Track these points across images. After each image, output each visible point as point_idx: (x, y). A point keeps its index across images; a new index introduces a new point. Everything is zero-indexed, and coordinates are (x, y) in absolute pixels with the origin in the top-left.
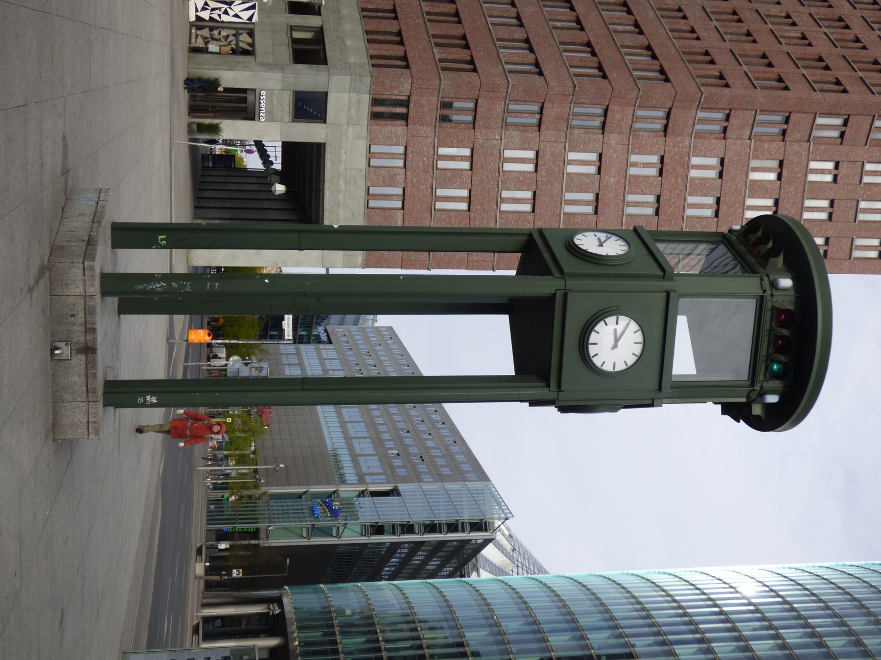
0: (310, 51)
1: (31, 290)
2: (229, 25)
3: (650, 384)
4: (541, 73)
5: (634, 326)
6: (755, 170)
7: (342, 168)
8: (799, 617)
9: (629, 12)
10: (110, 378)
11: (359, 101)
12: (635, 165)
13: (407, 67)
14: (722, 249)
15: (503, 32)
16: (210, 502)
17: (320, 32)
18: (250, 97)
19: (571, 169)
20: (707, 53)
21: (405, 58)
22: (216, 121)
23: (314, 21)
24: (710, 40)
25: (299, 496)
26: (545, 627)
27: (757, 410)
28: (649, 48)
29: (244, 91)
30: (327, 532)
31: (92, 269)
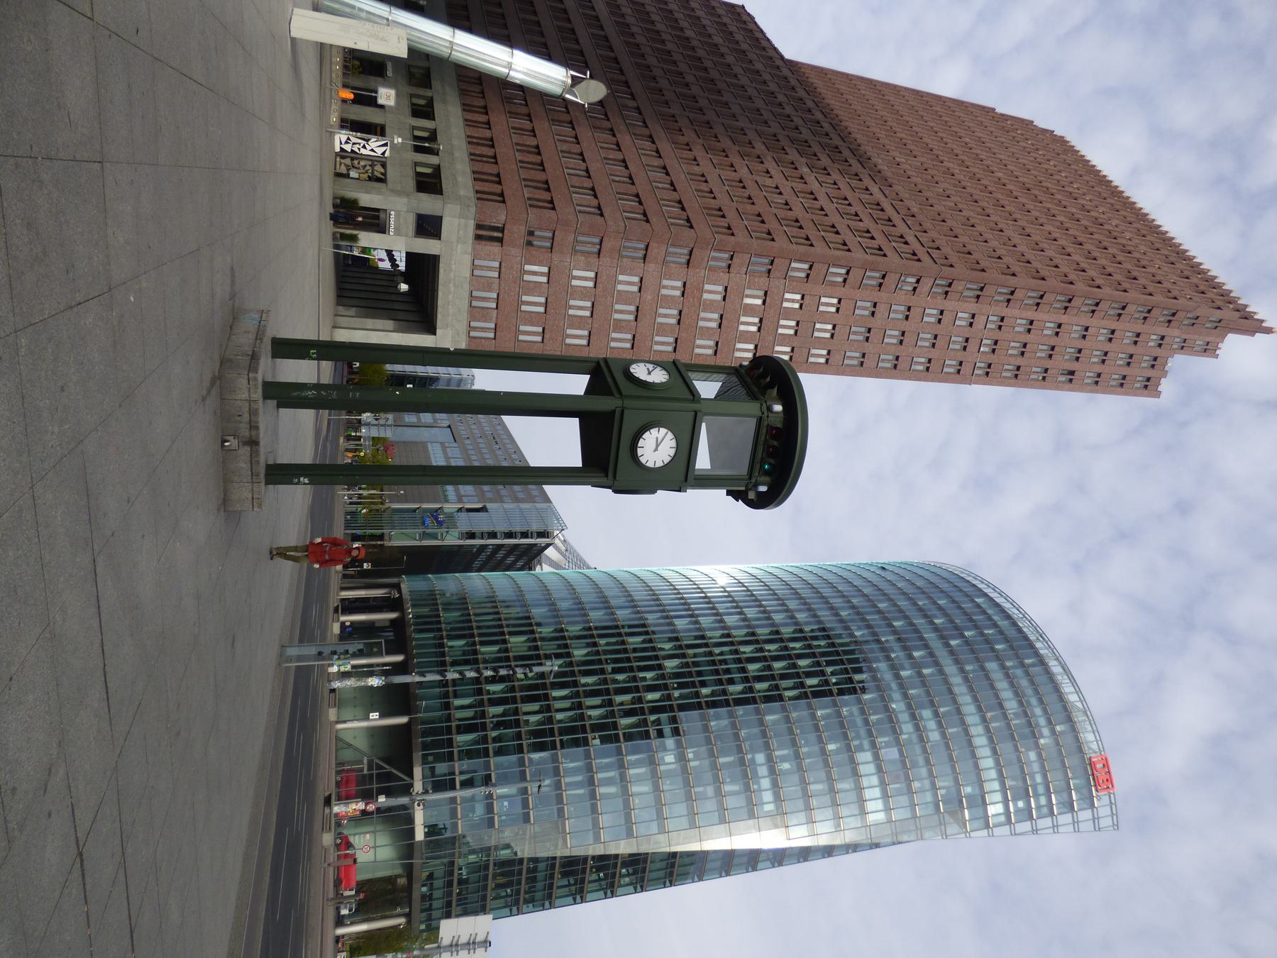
0: (429, 183)
1: (204, 399)
2: (367, 157)
3: (680, 475)
4: (602, 215)
5: (670, 435)
6: (748, 296)
7: (452, 275)
8: (757, 600)
9: (667, 174)
10: (271, 462)
11: (466, 226)
12: (665, 287)
13: (504, 202)
14: (734, 379)
15: (565, 147)
16: (347, 513)
17: (437, 169)
18: (382, 215)
19: (620, 287)
20: (720, 210)
21: (502, 195)
22: (355, 232)
23: (433, 160)
24: (723, 201)
25: (414, 510)
26: (587, 606)
27: (752, 495)
28: (680, 202)
29: (378, 210)
30: (434, 537)
31: (256, 379)
